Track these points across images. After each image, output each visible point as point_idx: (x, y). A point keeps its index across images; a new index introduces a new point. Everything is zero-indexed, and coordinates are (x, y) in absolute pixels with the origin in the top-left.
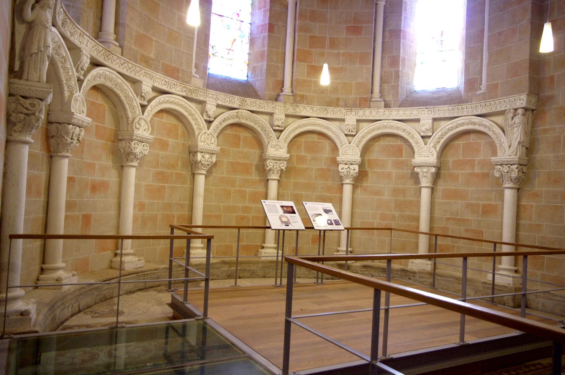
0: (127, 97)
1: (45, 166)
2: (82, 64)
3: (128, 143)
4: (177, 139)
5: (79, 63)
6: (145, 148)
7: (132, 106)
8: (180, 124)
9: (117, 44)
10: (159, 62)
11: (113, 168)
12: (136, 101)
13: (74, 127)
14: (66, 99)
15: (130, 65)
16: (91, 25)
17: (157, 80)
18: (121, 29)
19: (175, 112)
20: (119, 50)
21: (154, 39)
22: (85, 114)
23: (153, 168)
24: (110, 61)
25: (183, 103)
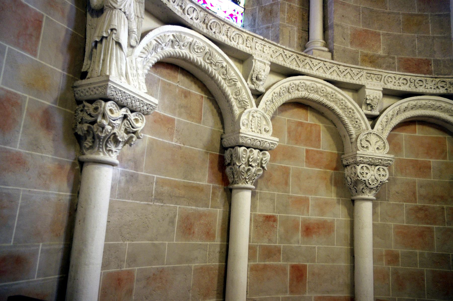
0: (345, 108)
1: (220, 199)
2: (256, 72)
3: (353, 169)
4: (445, 158)
5: (252, 72)
6: (382, 173)
7: (356, 122)
8: (447, 136)
9: (326, 49)
10: (393, 58)
11: (338, 203)
12: (359, 112)
13: (248, 150)
14: (237, 118)
15: (342, 68)
16: (296, 40)
17: (390, 80)
18: (330, 32)
19: (432, 120)
20: (329, 55)
21: (381, 32)
22: (271, 133)
23: (407, 201)
24: (308, 67)
25: (444, 105)
